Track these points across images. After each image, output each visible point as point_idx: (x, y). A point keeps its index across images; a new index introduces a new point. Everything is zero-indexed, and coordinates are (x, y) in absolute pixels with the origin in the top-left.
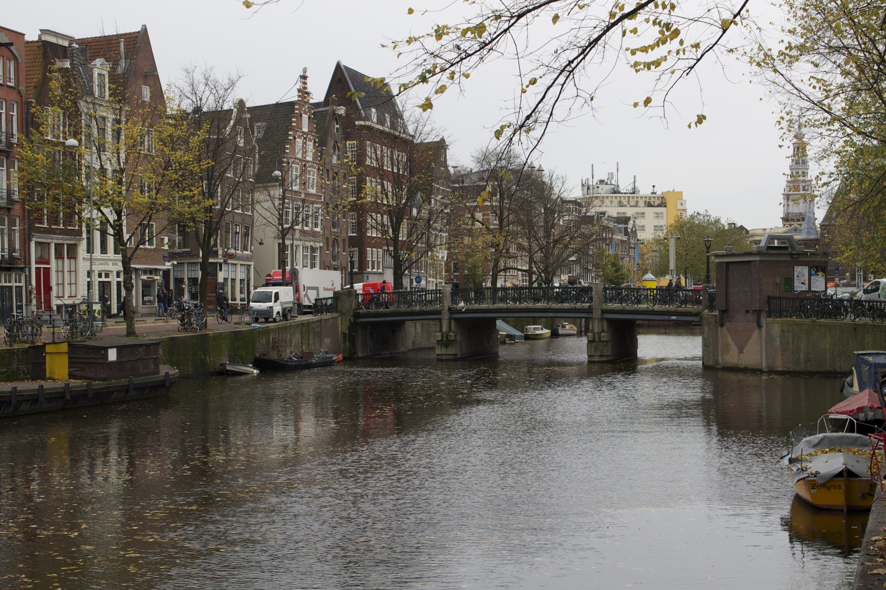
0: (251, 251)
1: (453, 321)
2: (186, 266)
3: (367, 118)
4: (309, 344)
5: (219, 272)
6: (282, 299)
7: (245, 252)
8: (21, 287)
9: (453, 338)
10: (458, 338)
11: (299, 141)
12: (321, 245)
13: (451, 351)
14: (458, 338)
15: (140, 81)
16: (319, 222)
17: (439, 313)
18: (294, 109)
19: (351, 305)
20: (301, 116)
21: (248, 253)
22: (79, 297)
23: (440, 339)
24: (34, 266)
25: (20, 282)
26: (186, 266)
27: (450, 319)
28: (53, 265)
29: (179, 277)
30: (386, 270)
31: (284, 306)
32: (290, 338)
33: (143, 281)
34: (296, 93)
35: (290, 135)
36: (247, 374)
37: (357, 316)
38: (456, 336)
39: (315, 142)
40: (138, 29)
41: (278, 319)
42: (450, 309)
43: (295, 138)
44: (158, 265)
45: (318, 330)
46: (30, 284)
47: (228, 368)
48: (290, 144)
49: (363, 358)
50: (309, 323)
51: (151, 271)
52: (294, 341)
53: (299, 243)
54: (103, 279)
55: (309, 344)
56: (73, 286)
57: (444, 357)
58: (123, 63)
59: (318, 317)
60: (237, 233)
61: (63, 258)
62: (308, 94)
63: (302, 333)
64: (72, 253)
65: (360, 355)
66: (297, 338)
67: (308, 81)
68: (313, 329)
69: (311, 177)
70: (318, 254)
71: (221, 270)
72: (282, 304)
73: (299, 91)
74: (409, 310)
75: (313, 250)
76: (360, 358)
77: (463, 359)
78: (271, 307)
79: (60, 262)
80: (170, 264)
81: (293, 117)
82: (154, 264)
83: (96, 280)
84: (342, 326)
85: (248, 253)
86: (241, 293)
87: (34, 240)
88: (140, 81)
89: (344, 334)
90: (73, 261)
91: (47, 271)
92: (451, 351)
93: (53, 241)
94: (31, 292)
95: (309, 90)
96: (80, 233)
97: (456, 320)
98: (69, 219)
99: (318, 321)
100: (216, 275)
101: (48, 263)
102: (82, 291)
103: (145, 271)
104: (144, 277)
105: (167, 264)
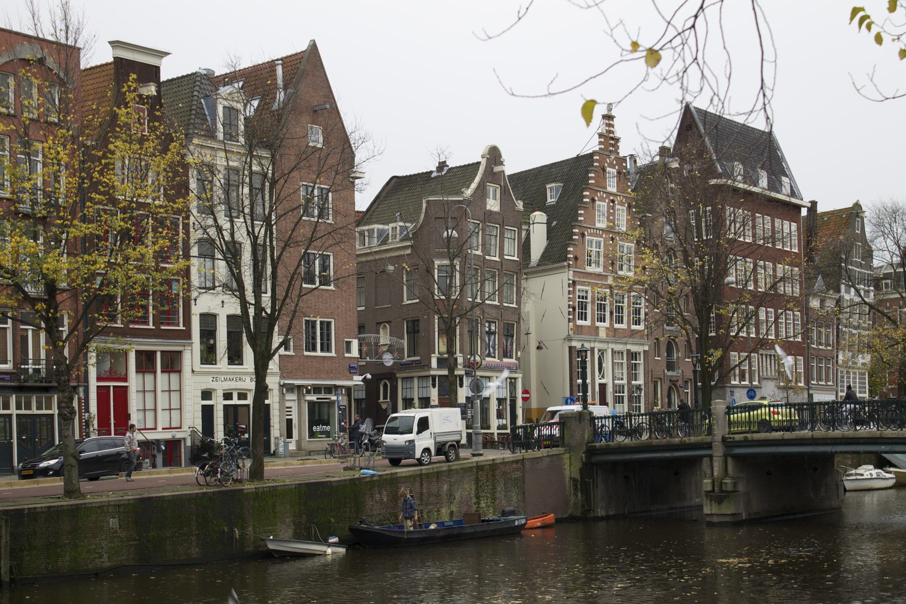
0: (517, 359)
1: (730, 460)
2: (416, 380)
3: (729, 175)
4: (494, 499)
5: (459, 388)
6: (436, 426)
7: (505, 360)
8: (53, 415)
9: (730, 488)
10: (741, 487)
11: (602, 205)
12: (646, 348)
13: (727, 509)
14: (741, 487)
15: (305, 118)
16: (642, 316)
17: (709, 446)
18: (593, 161)
19: (583, 435)
20: (604, 170)
21: (513, 361)
22: (185, 428)
23: (709, 488)
24: (93, 384)
25: (49, 407)
26: (416, 380)
27: (725, 456)
28: (134, 381)
29: (408, 397)
30: (764, 383)
31: (439, 439)
32: (450, 490)
33: (311, 404)
34: (596, 140)
35: (586, 196)
36: (312, 555)
37: (591, 452)
38: (735, 484)
39: (630, 206)
40: (303, 46)
41: (426, 459)
42: (724, 439)
43: (593, 200)
44: (339, 379)
45: (518, 474)
46: (87, 411)
47: (271, 546)
48: (585, 208)
49: (607, 518)
50: (494, 466)
51: (329, 389)
52: (458, 495)
53: (842, 369)
54: (235, 401)
55: (494, 499)
56: (175, 414)
57: (715, 520)
58: (281, 96)
59: (520, 454)
60: (490, 333)
61: (155, 372)
62: (617, 140)
63: (477, 481)
64: (172, 364)
65: (601, 512)
66: (466, 489)
67: (616, 122)
68: (505, 473)
69: (594, 249)
70: (641, 361)
71: (461, 386)
72: (435, 435)
73: (600, 135)
74: (664, 442)
75: (633, 356)
76: (602, 519)
77: (752, 522)
78: (412, 442)
79: (149, 378)
80: (361, 378)
81: (591, 172)
82: (332, 379)
83: (218, 403)
84: (571, 467)
85: (513, 361)
86: (500, 415)
87: (93, 345)
88: (305, 118)
89: (574, 480)
90: (174, 377)
91: (122, 395)
92: (727, 509)
93: (132, 348)
94: (88, 424)
95: (617, 135)
96: (186, 335)
97: (736, 457)
98: (166, 316)
99: (517, 462)
100: (456, 393)
101: (125, 379)
102: (193, 420)
103: (317, 389)
104: (313, 398)
105: (356, 378)
